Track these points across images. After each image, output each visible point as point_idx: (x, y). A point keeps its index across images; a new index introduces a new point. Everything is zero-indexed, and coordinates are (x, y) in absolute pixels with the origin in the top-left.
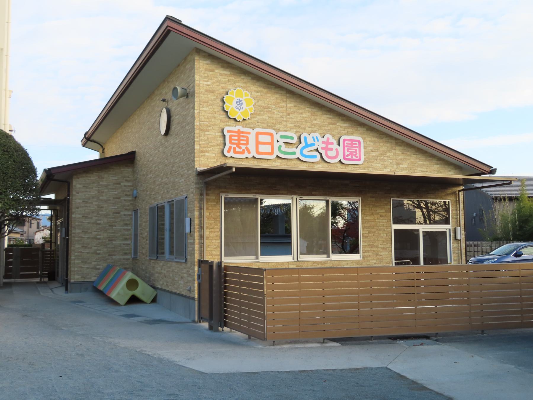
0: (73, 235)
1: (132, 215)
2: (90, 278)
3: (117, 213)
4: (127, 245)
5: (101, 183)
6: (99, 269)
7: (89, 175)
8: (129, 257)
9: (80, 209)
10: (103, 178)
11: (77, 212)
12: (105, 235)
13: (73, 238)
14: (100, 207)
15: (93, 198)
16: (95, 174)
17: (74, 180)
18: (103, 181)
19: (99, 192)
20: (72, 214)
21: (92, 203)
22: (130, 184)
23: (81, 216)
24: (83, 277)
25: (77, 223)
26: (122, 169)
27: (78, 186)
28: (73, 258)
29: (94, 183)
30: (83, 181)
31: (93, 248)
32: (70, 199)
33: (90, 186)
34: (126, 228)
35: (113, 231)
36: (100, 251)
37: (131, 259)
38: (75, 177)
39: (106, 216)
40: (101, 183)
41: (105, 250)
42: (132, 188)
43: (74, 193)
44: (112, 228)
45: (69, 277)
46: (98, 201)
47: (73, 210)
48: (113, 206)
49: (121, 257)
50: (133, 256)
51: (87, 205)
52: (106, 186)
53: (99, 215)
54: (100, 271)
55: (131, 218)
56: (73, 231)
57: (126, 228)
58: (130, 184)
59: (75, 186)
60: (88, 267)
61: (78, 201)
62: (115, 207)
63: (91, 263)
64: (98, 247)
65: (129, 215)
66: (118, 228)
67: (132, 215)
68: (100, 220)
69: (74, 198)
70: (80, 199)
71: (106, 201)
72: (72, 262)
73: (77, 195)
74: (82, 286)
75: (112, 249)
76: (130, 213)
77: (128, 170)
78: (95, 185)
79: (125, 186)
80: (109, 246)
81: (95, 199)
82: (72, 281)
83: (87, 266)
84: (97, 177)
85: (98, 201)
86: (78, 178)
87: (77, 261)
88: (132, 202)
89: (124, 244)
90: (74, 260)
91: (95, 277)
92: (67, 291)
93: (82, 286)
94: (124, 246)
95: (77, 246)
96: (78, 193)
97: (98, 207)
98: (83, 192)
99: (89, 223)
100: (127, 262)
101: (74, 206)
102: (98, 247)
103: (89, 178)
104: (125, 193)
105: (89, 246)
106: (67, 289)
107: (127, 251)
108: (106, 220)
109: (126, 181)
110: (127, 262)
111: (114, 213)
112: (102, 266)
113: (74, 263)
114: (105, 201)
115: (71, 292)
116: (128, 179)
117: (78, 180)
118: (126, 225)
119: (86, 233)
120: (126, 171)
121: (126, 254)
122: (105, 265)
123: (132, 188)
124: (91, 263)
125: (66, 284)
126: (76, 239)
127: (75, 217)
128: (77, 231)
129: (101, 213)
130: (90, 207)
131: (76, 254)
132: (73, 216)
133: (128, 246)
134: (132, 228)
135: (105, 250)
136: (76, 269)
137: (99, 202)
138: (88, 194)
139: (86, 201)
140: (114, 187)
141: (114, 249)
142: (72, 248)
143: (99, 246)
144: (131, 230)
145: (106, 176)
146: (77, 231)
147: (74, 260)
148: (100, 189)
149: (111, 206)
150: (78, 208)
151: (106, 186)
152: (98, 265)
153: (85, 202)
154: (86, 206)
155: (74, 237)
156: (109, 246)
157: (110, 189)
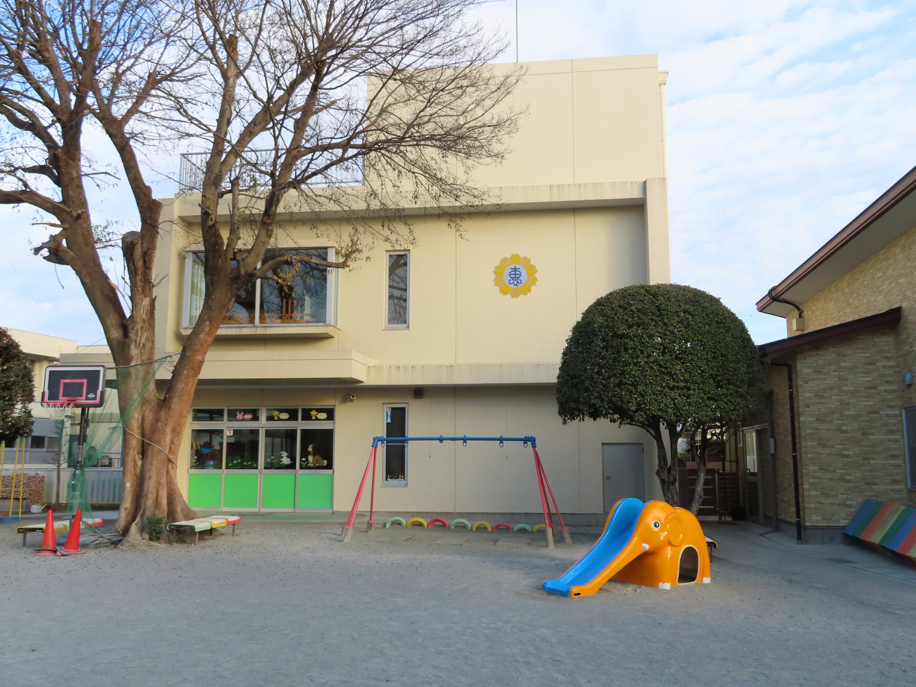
0: (803, 450)
1: (901, 415)
2: (838, 521)
3: (872, 388)
4: (899, 491)
5: (842, 364)
6: (850, 506)
7: (821, 352)
8: (901, 487)
9: (810, 384)
10: (845, 356)
11: (806, 413)
12: (857, 450)
13: (803, 456)
14: (845, 404)
15: (832, 388)
16: (831, 349)
17: (798, 361)
18: (845, 361)
19: (840, 380)
20: (799, 415)
21: (828, 373)
22: (892, 363)
23: (812, 395)
24: (820, 420)
25: (808, 431)
26: (876, 340)
27: (806, 371)
28: (806, 486)
29: (830, 364)
30: (812, 363)
31: (835, 422)
32: (802, 521)
33: (825, 371)
34: (895, 487)
35: (870, 444)
36: (853, 501)
37: (906, 490)
38: (799, 356)
39: (855, 417)
40: (842, 364)
41: (859, 475)
42: (897, 369)
43: (800, 382)
44: (869, 463)
45: (802, 518)
46: (842, 418)
47: (801, 410)
48: (863, 377)
49: (885, 462)
50: (909, 486)
51: (822, 401)
52: (852, 369)
53: (842, 392)
54: (853, 510)
55: (901, 422)
56: (803, 444)
57: (895, 487)
58: (892, 363)
59: (801, 371)
60: (832, 502)
61: (807, 395)
62: (867, 379)
63: (833, 446)
64: (841, 395)
65: (895, 415)
66: (881, 487)
67: (902, 416)
68: (846, 425)
69: (800, 390)
70: (810, 392)
71: (853, 393)
72: (806, 493)
73: (805, 385)
74: (825, 533)
75: (870, 473)
76: (896, 412)
77: (887, 340)
78: (833, 368)
79: (887, 415)
80: (865, 468)
81: (837, 416)
82: (808, 524)
83: (830, 500)
84: (835, 355)
85: (842, 418)
86: (805, 359)
87: (813, 493)
88: (898, 394)
89: (890, 465)
90: (809, 489)
91: (846, 519)
92: (800, 541)
93: (825, 533)
94: (891, 468)
95: (812, 468)
96: (806, 382)
97: (841, 404)
98: (816, 403)
99: (827, 430)
100: (898, 496)
101: (801, 403)
102: (841, 395)
103: (823, 358)
104: (884, 379)
105: (831, 468)
106: (799, 538)
107: (895, 453)
108: (855, 425)
109: (886, 358)
110: (898, 496)
111: (867, 388)
112: (857, 501)
113: (809, 496)
114: (854, 418)
115: (807, 543)
116: (888, 355)
117: (803, 361)
118: (892, 432)
119: (827, 495)
120: (885, 342)
121: (895, 482)
122: (861, 500)
123: (897, 369)
124: (833, 446)
125: (801, 532)
126: (809, 456)
127: (805, 421)
128: (810, 443)
129: (846, 413)
130: (827, 403)
131: (811, 480)
132: (802, 419)
133: (895, 444)
134: (903, 438)
135: (859, 475)
136: (813, 505)
137: (842, 420)
138: (823, 384)
139: (821, 394)
140: (868, 419)
141: (871, 449)
142: (804, 471)
143: (850, 492)
144: (902, 440)
145: (849, 352)
146: (810, 443)
147: (809, 489)
148: (841, 373)
149: (863, 401)
150: (808, 406)
151: (852, 369)
152: (849, 499)
153: (820, 420)
154: (819, 379)
155: (805, 453)
156: (865, 468)
157: (860, 396)
